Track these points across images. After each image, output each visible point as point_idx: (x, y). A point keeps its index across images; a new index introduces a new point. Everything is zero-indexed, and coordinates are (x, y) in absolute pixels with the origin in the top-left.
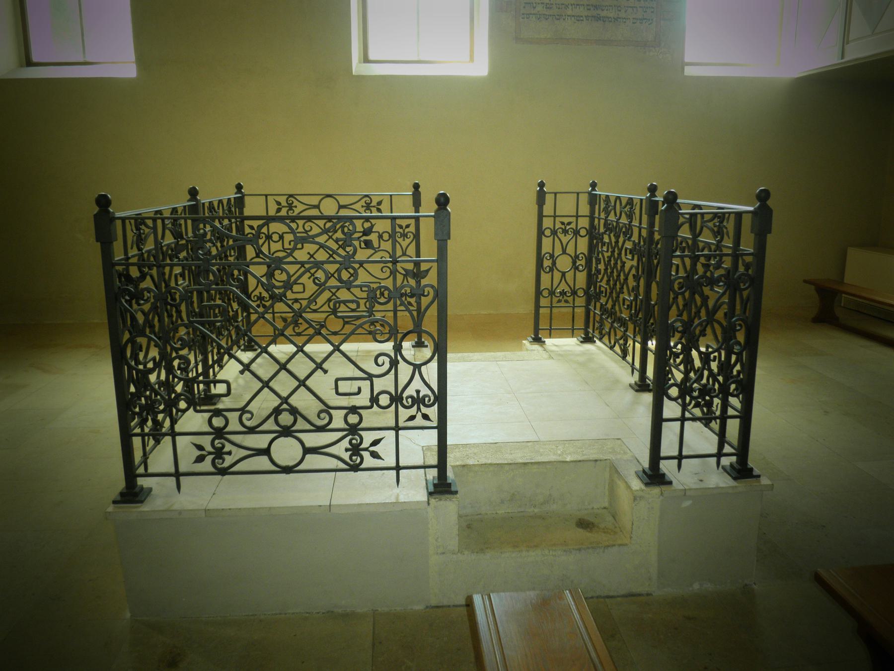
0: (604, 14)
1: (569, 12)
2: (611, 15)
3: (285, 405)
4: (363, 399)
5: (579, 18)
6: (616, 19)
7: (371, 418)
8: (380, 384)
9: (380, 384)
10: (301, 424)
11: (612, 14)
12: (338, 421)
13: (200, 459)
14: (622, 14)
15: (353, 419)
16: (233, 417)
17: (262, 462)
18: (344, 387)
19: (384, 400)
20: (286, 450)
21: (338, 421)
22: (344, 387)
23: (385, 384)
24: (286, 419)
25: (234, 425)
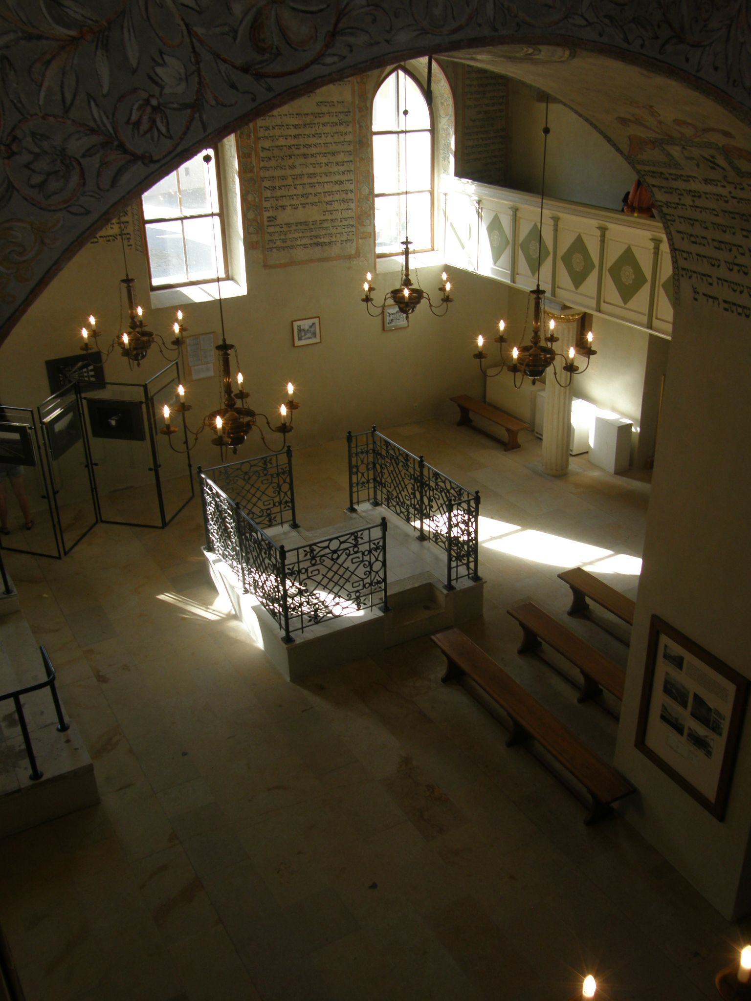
0: (322, 240)
1: (299, 243)
2: (326, 241)
3: (334, 561)
4: (310, 570)
5: (305, 246)
6: (330, 243)
7: (308, 564)
8: (366, 581)
9: (366, 581)
10: (330, 556)
11: (327, 240)
12: (318, 559)
13: (306, 555)
14: (334, 239)
15: (313, 562)
16: (352, 552)
17: (342, 539)
18: (316, 572)
19: (303, 571)
20: (334, 545)
21: (318, 559)
22: (316, 572)
23: (368, 580)
24: (335, 556)
25: (351, 549)
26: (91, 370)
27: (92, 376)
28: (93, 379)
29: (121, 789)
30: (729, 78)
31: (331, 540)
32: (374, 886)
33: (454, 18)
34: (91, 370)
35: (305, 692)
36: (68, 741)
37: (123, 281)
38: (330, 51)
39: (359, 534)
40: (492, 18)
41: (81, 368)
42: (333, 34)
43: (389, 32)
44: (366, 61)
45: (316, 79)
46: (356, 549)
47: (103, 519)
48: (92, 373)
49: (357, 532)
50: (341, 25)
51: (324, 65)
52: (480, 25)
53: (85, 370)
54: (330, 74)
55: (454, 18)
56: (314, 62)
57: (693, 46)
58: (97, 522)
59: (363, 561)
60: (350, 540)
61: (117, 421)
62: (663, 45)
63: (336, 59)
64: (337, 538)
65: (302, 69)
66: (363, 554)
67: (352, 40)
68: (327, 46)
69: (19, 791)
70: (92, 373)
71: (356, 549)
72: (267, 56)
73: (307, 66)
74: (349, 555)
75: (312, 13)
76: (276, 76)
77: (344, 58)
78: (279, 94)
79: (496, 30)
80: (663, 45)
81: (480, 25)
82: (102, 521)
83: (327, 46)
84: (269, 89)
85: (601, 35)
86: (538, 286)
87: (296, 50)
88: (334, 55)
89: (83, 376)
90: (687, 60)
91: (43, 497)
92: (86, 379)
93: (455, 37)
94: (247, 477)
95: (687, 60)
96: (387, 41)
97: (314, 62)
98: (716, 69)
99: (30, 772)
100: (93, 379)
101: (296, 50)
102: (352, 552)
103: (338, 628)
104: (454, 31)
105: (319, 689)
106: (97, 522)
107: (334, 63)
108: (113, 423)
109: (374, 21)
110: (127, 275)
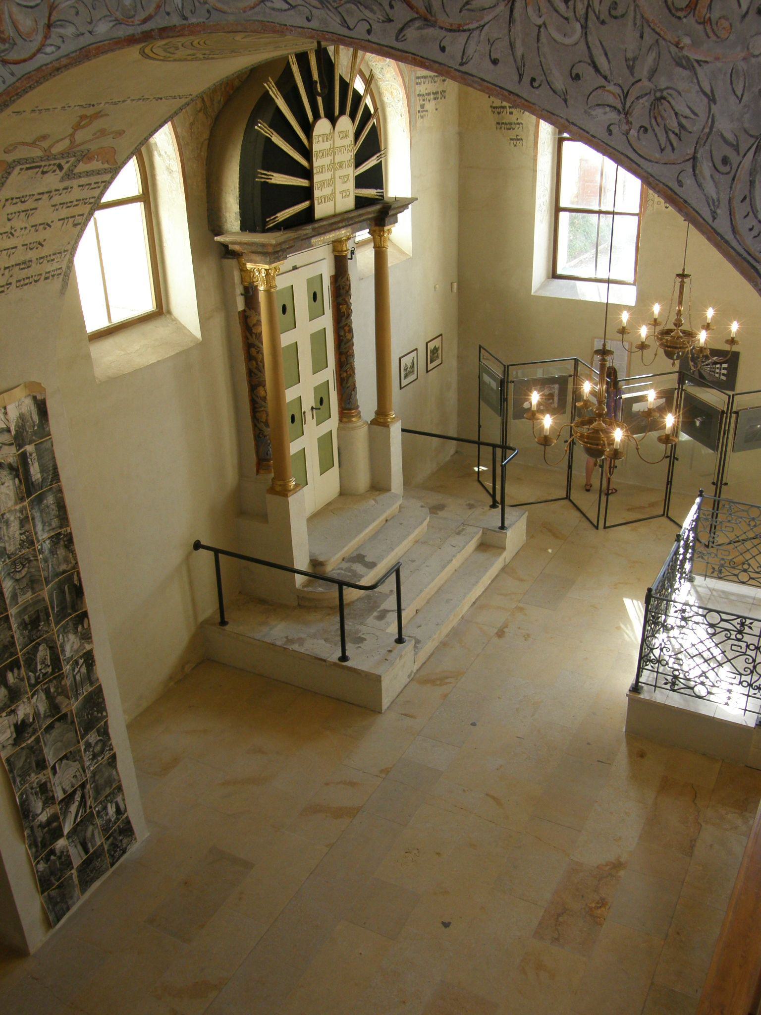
16: (733, 637)
17: (724, 616)
26: (724, 369)
27: (723, 375)
28: (724, 378)
29: (405, 715)
30: (521, 76)
31: (710, 610)
32: (446, 925)
33: (143, 7)
34: (724, 369)
35: (624, 748)
36: (390, 651)
37: (678, 275)
38: (49, 42)
39: (748, 621)
40: (180, 6)
41: (715, 363)
42: (49, 26)
43: (90, 23)
44: (76, 51)
45: (41, 66)
46: (739, 636)
47: (669, 515)
48: (725, 372)
49: (745, 618)
50: (52, 18)
51: (46, 54)
52: (168, 14)
53: (718, 366)
54: (51, 62)
55: (143, 7)
56: (39, 51)
57: (451, 31)
58: (663, 515)
59: (745, 654)
60: (734, 622)
61: (701, 423)
62: (402, 30)
63: (53, 48)
64: (718, 612)
65: (31, 58)
66: (748, 646)
67: (61, 31)
68: (46, 37)
69: (325, 661)
70: (725, 372)
71: (739, 636)
72: (7, 45)
73: (34, 55)
74: (729, 638)
75: (31, 7)
76: (16, 63)
77: (59, 48)
78: (20, 79)
79: (186, 19)
80: (402, 30)
81: (168, 14)
82: (668, 517)
83: (46, 37)
84: (13, 74)
85: (308, 20)
86: (604, 345)
87: (25, 40)
88: (52, 45)
89: (714, 372)
90: (443, 49)
91: (713, 483)
92: (717, 375)
93: (147, 27)
94: (752, 523)
95: (443, 49)
96: (90, 32)
97: (39, 51)
98: (495, 62)
99: (340, 654)
100: (724, 378)
101: (25, 40)
102: (733, 637)
103: (653, 700)
104: (145, 21)
105: (638, 755)
106: (663, 515)
107: (53, 53)
108: (698, 423)
109: (77, 13)
110: (684, 270)
